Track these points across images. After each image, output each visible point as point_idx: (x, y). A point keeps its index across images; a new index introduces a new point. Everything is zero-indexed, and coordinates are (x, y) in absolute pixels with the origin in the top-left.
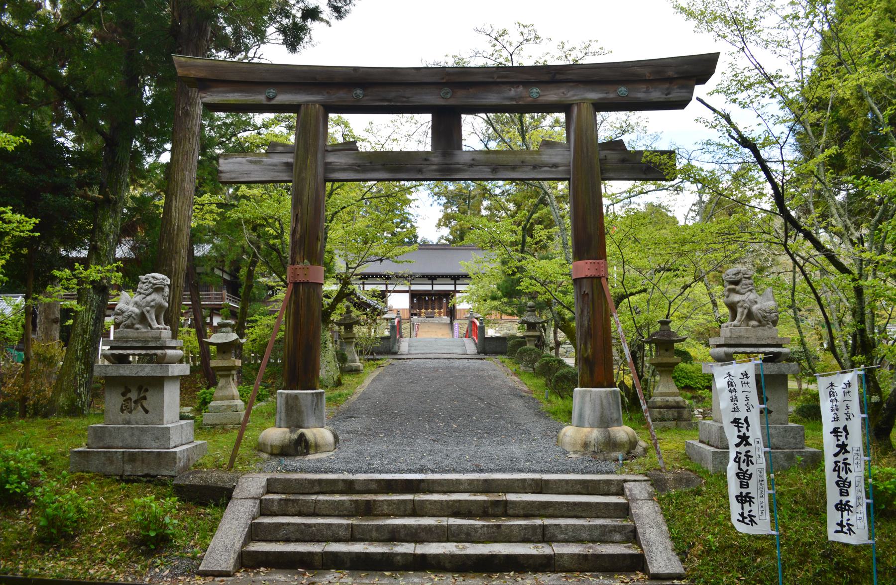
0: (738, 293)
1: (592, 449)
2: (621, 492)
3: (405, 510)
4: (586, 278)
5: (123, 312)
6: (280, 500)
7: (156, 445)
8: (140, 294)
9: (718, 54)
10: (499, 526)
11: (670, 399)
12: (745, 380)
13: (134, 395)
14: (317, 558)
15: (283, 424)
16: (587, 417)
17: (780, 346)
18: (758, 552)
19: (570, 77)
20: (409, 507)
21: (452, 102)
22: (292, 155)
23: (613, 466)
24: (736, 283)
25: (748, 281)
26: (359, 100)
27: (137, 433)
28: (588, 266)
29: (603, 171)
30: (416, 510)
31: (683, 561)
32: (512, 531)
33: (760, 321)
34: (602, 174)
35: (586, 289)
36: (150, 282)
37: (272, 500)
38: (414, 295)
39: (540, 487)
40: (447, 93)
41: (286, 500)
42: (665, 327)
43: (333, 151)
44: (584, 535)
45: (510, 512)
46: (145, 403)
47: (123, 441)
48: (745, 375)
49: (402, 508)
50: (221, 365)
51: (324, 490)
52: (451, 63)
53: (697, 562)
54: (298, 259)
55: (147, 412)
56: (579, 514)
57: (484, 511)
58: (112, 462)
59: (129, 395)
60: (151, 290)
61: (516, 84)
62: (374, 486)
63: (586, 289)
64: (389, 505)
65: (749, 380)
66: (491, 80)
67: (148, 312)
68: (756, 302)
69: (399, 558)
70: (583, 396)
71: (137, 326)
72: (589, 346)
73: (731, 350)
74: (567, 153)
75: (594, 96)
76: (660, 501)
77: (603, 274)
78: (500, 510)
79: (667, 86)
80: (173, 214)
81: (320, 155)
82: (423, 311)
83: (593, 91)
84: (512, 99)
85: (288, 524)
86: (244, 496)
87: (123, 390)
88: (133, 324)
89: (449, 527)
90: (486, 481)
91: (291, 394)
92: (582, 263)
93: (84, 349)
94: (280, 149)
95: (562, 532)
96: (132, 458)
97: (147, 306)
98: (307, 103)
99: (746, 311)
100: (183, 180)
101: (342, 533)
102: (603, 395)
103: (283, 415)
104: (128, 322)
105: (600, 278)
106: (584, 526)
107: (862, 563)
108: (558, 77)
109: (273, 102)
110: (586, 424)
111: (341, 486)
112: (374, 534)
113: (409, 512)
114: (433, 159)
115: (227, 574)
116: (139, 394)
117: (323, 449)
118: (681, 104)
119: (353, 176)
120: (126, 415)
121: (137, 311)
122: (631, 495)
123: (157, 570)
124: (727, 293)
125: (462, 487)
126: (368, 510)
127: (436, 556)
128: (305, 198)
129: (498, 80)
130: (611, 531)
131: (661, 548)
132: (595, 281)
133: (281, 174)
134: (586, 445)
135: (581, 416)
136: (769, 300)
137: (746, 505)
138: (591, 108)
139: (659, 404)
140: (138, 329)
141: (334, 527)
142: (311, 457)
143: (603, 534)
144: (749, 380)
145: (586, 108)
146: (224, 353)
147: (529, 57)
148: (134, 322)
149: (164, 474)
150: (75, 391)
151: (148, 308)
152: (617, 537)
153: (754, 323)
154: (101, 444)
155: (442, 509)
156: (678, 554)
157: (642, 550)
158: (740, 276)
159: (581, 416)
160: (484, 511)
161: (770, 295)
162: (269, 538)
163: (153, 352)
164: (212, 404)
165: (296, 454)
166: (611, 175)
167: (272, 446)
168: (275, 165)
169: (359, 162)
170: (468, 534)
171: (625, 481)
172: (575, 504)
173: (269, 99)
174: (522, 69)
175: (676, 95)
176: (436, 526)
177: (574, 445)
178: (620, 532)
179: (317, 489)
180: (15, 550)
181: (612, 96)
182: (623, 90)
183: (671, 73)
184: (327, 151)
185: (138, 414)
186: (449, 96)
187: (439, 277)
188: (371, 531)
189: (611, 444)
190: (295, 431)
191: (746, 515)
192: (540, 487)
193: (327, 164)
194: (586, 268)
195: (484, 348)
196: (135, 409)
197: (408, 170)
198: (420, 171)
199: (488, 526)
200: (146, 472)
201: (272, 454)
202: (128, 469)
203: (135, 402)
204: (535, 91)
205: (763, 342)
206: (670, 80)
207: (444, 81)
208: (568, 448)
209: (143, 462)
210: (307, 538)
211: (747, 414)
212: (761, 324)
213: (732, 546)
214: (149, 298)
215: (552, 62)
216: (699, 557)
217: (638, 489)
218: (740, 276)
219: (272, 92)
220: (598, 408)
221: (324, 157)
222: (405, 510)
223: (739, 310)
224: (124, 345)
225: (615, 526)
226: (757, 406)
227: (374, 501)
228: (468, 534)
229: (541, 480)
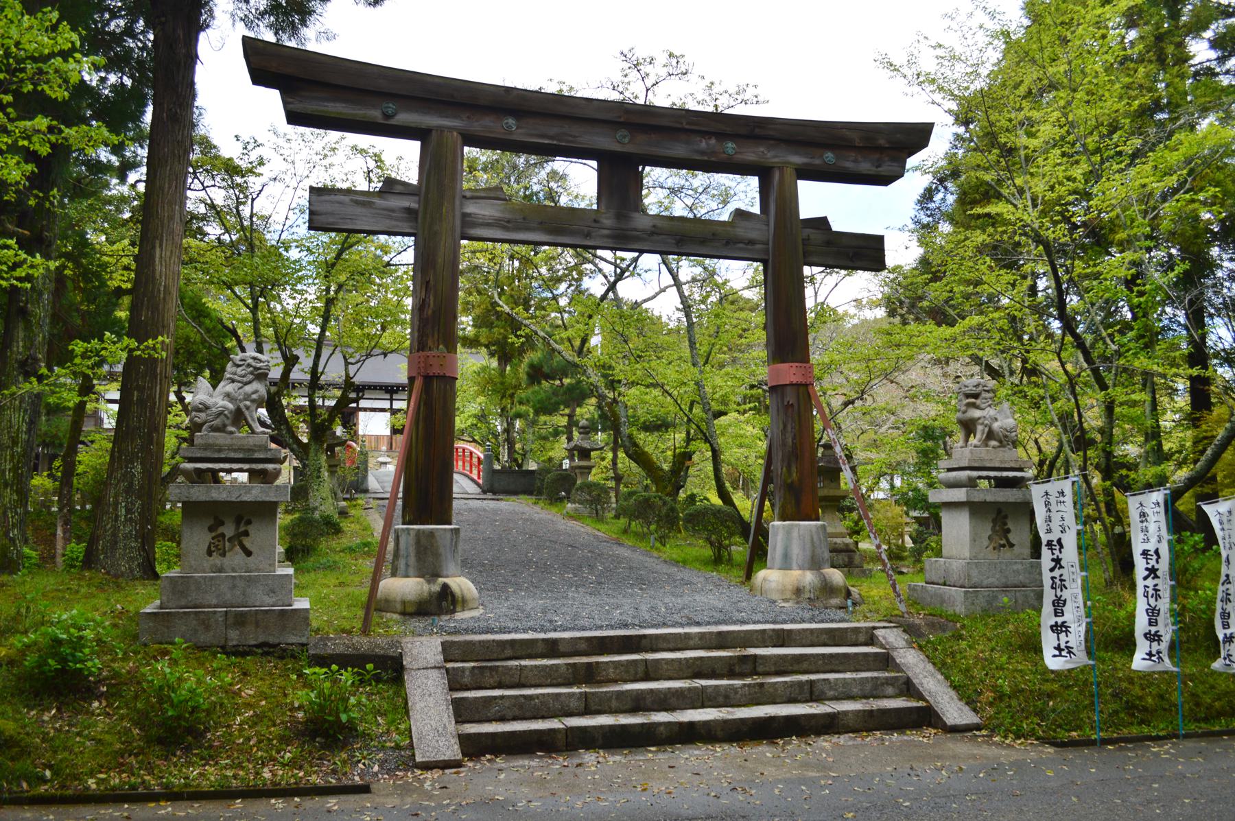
0: (978, 408)
1: (807, 595)
2: (871, 640)
3: (636, 673)
4: (791, 385)
5: (207, 408)
6: (474, 668)
7: (271, 601)
8: (233, 381)
10: (762, 685)
11: (838, 540)
12: (1062, 499)
13: (229, 530)
14: (559, 736)
15: (411, 571)
16: (794, 557)
17: (1021, 469)
18: (1050, 696)
19: (771, 133)
20: (641, 669)
21: (630, 149)
22: (416, 198)
23: (841, 613)
24: (976, 396)
26: (511, 133)
27: (241, 584)
28: (793, 370)
29: (805, 254)
30: (649, 672)
31: (975, 710)
32: (776, 690)
33: (1001, 442)
34: (804, 256)
35: (790, 398)
36: (249, 366)
37: (463, 669)
39: (782, 638)
40: (624, 137)
42: (829, 452)
43: (472, 198)
44: (855, 691)
45: (760, 669)
46: (247, 542)
47: (218, 596)
48: (1062, 493)
49: (632, 670)
51: (519, 654)
52: (551, 88)
53: (990, 711)
54: (430, 343)
55: (248, 553)
56: (836, 668)
57: (731, 669)
58: (207, 628)
59: (221, 530)
61: (707, 134)
62: (583, 646)
63: (790, 398)
64: (616, 668)
65: (1065, 499)
66: (679, 126)
67: (248, 408)
68: (996, 419)
69: (662, 728)
70: (788, 532)
71: (231, 429)
72: (794, 469)
73: (975, 474)
74: (765, 228)
75: (797, 159)
76: (921, 648)
78: (748, 667)
79: (877, 156)
80: (158, 268)
81: (457, 202)
83: (796, 153)
84: (703, 153)
85: (502, 697)
86: (421, 666)
87: (211, 522)
88: (225, 426)
89: (704, 688)
90: (720, 633)
91: (424, 531)
92: (784, 366)
93: (15, 469)
94: (399, 188)
95: (831, 689)
96: (240, 620)
97: (245, 399)
98: (441, 129)
100: (171, 218)
101: (574, 704)
102: (814, 530)
103: (412, 560)
104: (217, 422)
105: (806, 385)
106: (854, 679)
107: (1150, 700)
108: (757, 131)
109: (392, 122)
110: (794, 565)
111: (540, 648)
112: (614, 704)
113: (640, 675)
114: (605, 221)
115: (457, 764)
117: (471, 605)
119: (499, 234)
120: (216, 560)
121: (231, 406)
122: (888, 643)
123: (360, 765)
124: (964, 408)
125: (691, 643)
126: (589, 675)
127: (706, 723)
128: (440, 260)
130: (883, 684)
131: (946, 698)
132: (802, 389)
133: (400, 224)
134: (798, 591)
135: (786, 556)
136: (1007, 417)
137: (1063, 636)
140: (232, 433)
141: (563, 698)
142: (459, 616)
143: (875, 687)
144: (1065, 499)
145: (789, 172)
147: (667, 95)
148: (227, 422)
149: (290, 641)
150: (6, 534)
151: (248, 403)
152: (890, 690)
153: (993, 443)
154: (183, 602)
155: (681, 670)
156: (967, 703)
157: (927, 701)
158: (980, 388)
159: (786, 556)
160: (731, 669)
161: (1008, 412)
162: (477, 718)
163: (260, 466)
165: (440, 612)
166: (815, 259)
168: (392, 211)
169: (507, 216)
170: (727, 697)
171: (874, 628)
172: (831, 656)
174: (649, 110)
175: (885, 169)
176: (689, 689)
177: (782, 591)
178: (892, 685)
179: (508, 652)
180: (122, 757)
181: (817, 162)
182: (829, 156)
184: (464, 197)
185: (236, 557)
186: (626, 140)
188: (610, 699)
189: (827, 589)
190: (434, 582)
191: (1063, 646)
192: (782, 638)
193: (465, 215)
194: (789, 373)
195: (492, 486)
196: (231, 550)
197: (572, 233)
198: (588, 235)
199: (749, 685)
200: (262, 639)
201: (403, 613)
202: (234, 637)
204: (730, 146)
205: (1007, 465)
206: (880, 149)
208: (775, 597)
209: (257, 625)
210: (528, 714)
211: (1060, 535)
212: (1002, 445)
213: (1023, 690)
214: (248, 389)
215: (692, 106)
216: (991, 704)
217: (892, 637)
219: (391, 107)
220: (808, 546)
221: (462, 205)
222: (636, 673)
223: (980, 428)
224: (216, 455)
225: (887, 678)
226: (1073, 528)
227: (597, 663)
228: (727, 697)
229: (783, 630)
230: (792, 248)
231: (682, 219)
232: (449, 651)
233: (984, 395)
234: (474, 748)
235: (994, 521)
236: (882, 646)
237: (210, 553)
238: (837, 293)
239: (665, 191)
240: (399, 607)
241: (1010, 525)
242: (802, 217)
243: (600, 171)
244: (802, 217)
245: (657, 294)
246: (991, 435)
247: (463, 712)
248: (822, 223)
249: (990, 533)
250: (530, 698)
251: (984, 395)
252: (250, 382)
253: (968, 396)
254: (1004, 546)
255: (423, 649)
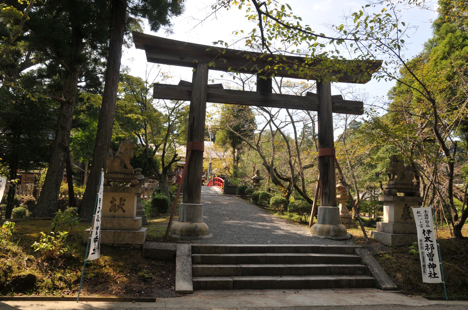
14: (231, 283)
230: (323, 105)
231: (167, 99)
232: (194, 250)
234: (198, 287)
236: (365, 265)
239: (282, 85)
242: (332, 95)
243: (209, 102)
244: (332, 95)
245: (285, 126)
247: (195, 273)
248: (339, 98)
250: (223, 268)
254: (408, 218)
255: (183, 249)
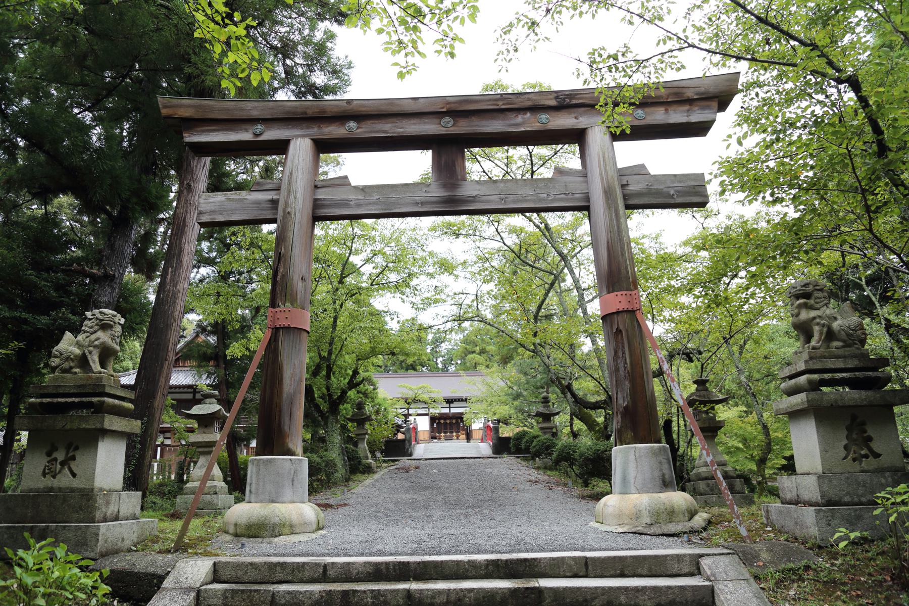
0: (812, 308)
2: (697, 571)
6: (226, 591)
9: (739, 73)
13: (60, 456)
19: (580, 101)
25: (820, 294)
36: (97, 319)
38: (433, 419)
40: (448, 123)
41: (234, 591)
46: (73, 465)
50: (201, 440)
59: (55, 455)
60: (96, 328)
64: (375, 597)
77: (636, 307)
82: (443, 434)
97: (89, 346)
99: (825, 329)
104: (66, 365)
110: (633, 489)
116: (67, 453)
118: (700, 129)
129: (503, 107)
135: (625, 480)
138: (607, 137)
139: (704, 475)
140: (76, 373)
146: (206, 426)
151: (91, 349)
158: (811, 287)
164: (188, 485)
167: (236, 525)
172: (637, 589)
173: (257, 135)
183: (690, 94)
187: (455, 400)
196: (60, 472)
201: (236, 535)
203: (63, 464)
207: (444, 110)
214: (93, 337)
218: (811, 287)
219: (259, 128)
223: (816, 329)
233: (816, 294)
235: (849, 429)
237: (44, 474)
238: (658, 232)
240: (232, 530)
241: (871, 431)
246: (830, 335)
249: (845, 442)
251: (816, 294)
252: (95, 332)
253: (797, 297)
254: (866, 456)
